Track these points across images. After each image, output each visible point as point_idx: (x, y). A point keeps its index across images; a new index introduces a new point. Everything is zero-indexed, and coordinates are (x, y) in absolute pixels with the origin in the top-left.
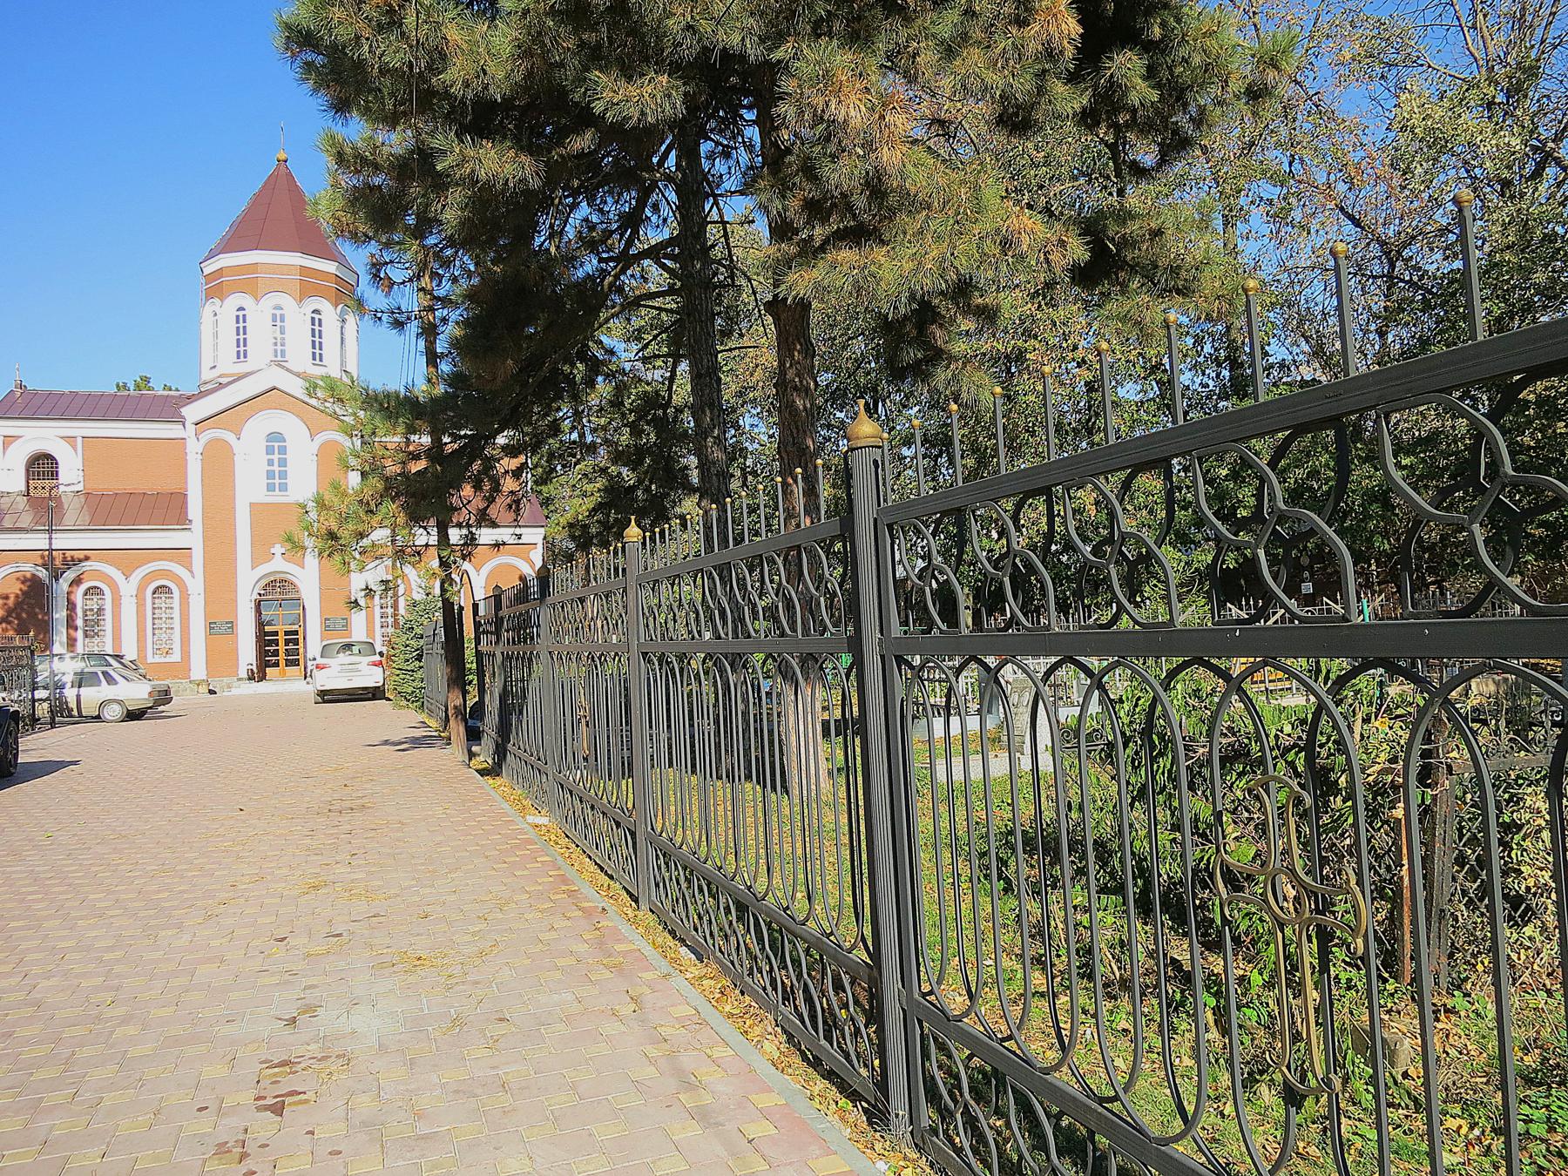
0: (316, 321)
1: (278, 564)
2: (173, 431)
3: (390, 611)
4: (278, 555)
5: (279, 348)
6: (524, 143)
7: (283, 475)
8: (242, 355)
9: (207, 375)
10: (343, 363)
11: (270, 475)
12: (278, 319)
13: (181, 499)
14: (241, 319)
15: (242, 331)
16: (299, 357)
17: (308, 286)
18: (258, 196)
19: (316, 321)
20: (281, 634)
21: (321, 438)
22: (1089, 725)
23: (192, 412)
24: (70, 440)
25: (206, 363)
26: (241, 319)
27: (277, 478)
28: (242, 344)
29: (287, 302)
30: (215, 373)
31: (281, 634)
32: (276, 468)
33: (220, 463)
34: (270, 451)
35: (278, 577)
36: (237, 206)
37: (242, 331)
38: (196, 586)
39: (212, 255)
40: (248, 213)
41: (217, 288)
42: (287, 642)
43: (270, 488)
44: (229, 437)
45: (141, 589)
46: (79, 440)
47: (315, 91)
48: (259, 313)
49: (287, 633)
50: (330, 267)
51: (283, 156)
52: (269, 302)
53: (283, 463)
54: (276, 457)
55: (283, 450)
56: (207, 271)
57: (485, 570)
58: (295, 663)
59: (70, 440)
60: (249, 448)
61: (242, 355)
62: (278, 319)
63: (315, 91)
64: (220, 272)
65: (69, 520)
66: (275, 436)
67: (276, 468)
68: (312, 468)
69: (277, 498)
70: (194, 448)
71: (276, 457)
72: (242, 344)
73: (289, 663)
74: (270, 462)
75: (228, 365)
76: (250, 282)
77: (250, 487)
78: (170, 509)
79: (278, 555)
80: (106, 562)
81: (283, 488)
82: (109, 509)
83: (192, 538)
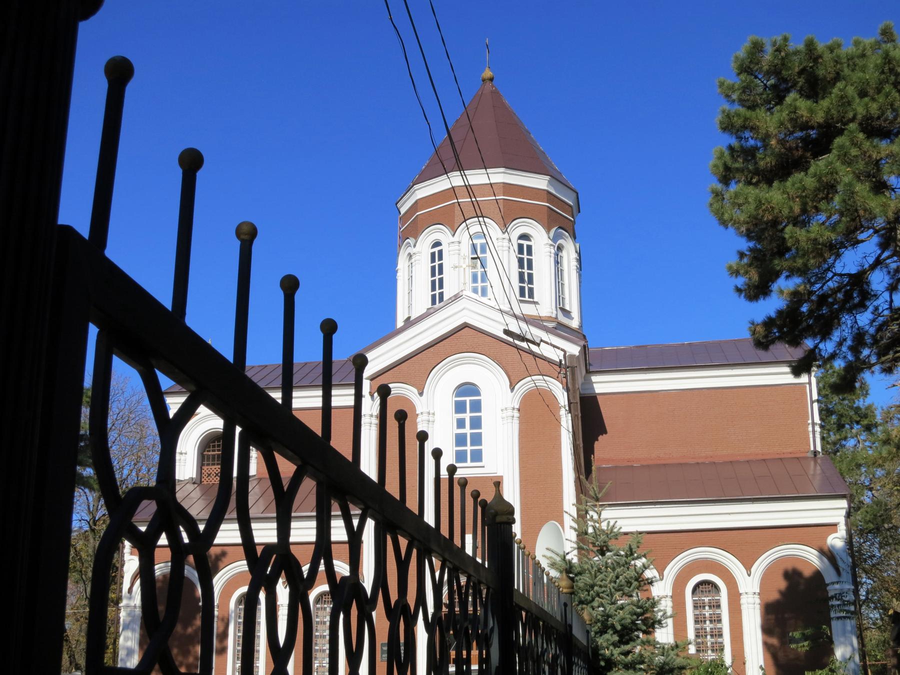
0: (524, 251)
6: (770, 121)
7: (477, 439)
14: (437, 256)
15: (437, 270)
19: (524, 251)
21: (525, 385)
22: (833, 257)
26: (437, 256)
29: (493, 229)
32: (467, 430)
34: (460, 408)
37: (437, 270)
40: (364, 369)
47: (781, 592)
48: (456, 245)
50: (540, 182)
51: (488, 73)
52: (463, 235)
53: (476, 423)
54: (467, 416)
55: (476, 406)
56: (403, 210)
63: (781, 592)
66: (468, 389)
67: (467, 430)
68: (513, 428)
71: (467, 416)
74: (461, 424)
76: (449, 213)
80: (258, 463)
81: (477, 456)
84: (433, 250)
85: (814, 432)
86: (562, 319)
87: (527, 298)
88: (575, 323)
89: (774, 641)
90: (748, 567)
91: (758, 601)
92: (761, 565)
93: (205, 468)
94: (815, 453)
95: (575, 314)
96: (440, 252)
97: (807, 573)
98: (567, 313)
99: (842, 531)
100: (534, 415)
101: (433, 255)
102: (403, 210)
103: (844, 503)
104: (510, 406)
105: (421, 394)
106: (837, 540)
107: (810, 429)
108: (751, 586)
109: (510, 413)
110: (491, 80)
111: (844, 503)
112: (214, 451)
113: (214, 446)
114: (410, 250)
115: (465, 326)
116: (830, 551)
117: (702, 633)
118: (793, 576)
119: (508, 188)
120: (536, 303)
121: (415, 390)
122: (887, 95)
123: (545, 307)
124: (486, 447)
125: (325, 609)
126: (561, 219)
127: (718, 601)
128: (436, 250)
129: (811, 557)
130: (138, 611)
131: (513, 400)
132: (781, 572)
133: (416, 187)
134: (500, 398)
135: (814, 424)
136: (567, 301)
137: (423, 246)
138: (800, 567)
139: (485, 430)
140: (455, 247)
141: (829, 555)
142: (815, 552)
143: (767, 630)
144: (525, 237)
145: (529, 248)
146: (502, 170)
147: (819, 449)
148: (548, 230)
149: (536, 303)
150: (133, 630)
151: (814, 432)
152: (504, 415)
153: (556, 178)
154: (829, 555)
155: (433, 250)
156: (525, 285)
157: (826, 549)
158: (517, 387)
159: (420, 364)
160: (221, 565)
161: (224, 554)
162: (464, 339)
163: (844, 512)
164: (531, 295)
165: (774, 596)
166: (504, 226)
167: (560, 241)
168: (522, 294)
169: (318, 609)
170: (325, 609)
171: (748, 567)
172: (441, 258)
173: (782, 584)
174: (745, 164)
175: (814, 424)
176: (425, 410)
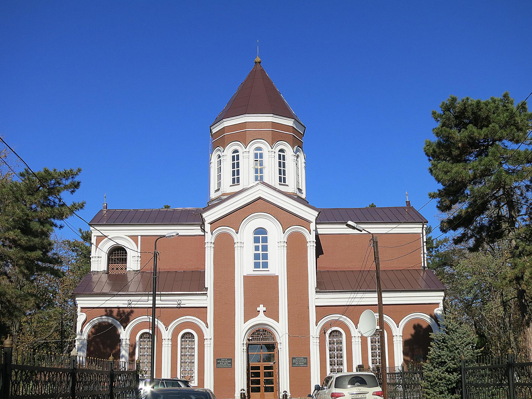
0: (282, 158)
1: (261, 319)
2: (196, 231)
3: (378, 351)
4: (262, 313)
5: (259, 175)
7: (265, 257)
8: (236, 181)
9: (213, 195)
10: (298, 183)
11: (257, 257)
12: (258, 157)
13: (202, 274)
14: (236, 158)
15: (236, 165)
16: (271, 174)
17: (275, 135)
18: (244, 85)
19: (282, 158)
20: (262, 368)
21: (289, 231)
23: (209, 216)
24: (134, 238)
25: (213, 186)
26: (236, 158)
27: (261, 259)
28: (236, 173)
29: (265, 146)
30: (219, 194)
31: (262, 368)
32: (260, 252)
33: (225, 249)
34: (256, 240)
35: (261, 327)
36: (232, 90)
37: (236, 165)
38: (209, 333)
39: (218, 120)
41: (221, 141)
42: (266, 375)
43: (257, 265)
44: (232, 231)
45: (323, 332)
46: (139, 237)
49: (266, 368)
50: (289, 122)
51: (258, 59)
52: (252, 147)
53: (265, 248)
54: (260, 244)
55: (265, 240)
56: (214, 131)
57: (402, 323)
58: (271, 390)
59: (134, 238)
60: (244, 238)
61: (236, 181)
62: (258, 157)
63: (412, 335)
64: (223, 130)
65: (132, 288)
67: (260, 252)
68: (284, 252)
69: (261, 272)
70: (209, 238)
71: (260, 244)
72: (236, 173)
73: (267, 390)
74: (257, 248)
75: (227, 187)
76: (242, 135)
77: (244, 265)
78: (194, 282)
79: (262, 313)
81: (265, 265)
82: (155, 281)
83: (207, 301)
84: (234, 154)
85: (424, 257)
86: (299, 194)
87: (282, 183)
88: (304, 196)
89: (408, 358)
90: (277, 319)
91: (402, 340)
92: (402, 323)
93: (110, 265)
94: (424, 267)
95: (304, 191)
96: (238, 156)
97: (424, 326)
98: (300, 190)
99: (441, 307)
100: (295, 246)
101: (233, 157)
102: (214, 131)
103: (443, 294)
104: (282, 240)
105: (237, 233)
106: (438, 311)
107: (422, 256)
108: (398, 332)
109: (282, 244)
110: (260, 63)
111: (443, 294)
112: (123, 256)
113: (115, 254)
114: (219, 153)
115: (260, 198)
116: (435, 316)
117: (375, 354)
118: (417, 327)
119: (274, 125)
120: (287, 185)
121: (234, 231)
122: (512, 130)
123: (291, 188)
124: (270, 261)
125: (145, 341)
126: (297, 142)
127: (341, 340)
128: (235, 154)
129: (427, 318)
130: (86, 342)
131: (284, 238)
132: (412, 326)
133: (224, 120)
134: (277, 236)
135: (424, 253)
136: (300, 184)
137: (228, 152)
138: (421, 324)
139: (270, 252)
140: (246, 154)
141: (435, 318)
142: (429, 317)
143: (405, 353)
144: (282, 151)
145: (284, 156)
146: (271, 115)
147: (426, 265)
148: (293, 147)
149: (287, 185)
150: (83, 352)
151: (424, 257)
152: (279, 245)
153: (297, 121)
154: (435, 318)
155: (234, 154)
156: (259, 167)
157: (433, 315)
158: (286, 231)
159: (235, 218)
160: (131, 317)
161: (132, 312)
162: (259, 205)
163: (442, 298)
164: (285, 182)
165: (409, 337)
166: (272, 143)
167: (298, 153)
168: (280, 181)
169: (141, 341)
170: (145, 341)
171: (277, 319)
172: (238, 159)
173: (413, 331)
174: (443, 151)
175: (424, 253)
176: (239, 241)
